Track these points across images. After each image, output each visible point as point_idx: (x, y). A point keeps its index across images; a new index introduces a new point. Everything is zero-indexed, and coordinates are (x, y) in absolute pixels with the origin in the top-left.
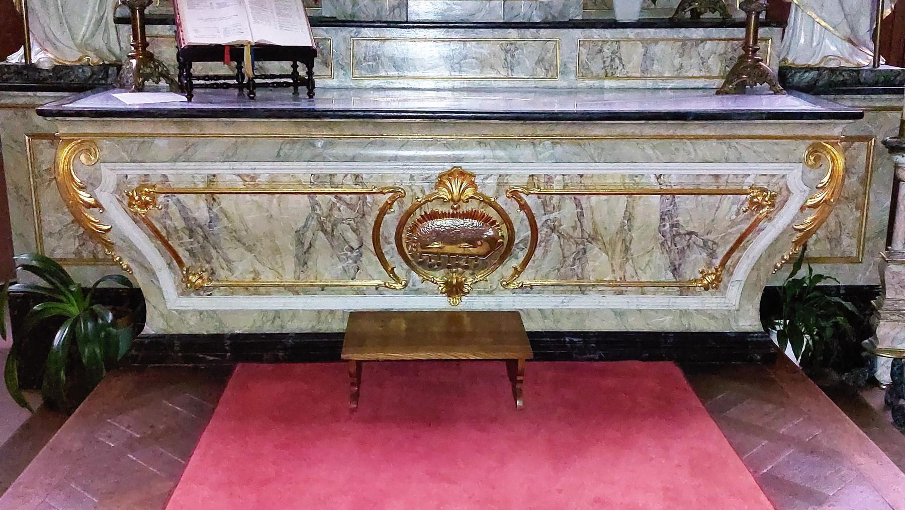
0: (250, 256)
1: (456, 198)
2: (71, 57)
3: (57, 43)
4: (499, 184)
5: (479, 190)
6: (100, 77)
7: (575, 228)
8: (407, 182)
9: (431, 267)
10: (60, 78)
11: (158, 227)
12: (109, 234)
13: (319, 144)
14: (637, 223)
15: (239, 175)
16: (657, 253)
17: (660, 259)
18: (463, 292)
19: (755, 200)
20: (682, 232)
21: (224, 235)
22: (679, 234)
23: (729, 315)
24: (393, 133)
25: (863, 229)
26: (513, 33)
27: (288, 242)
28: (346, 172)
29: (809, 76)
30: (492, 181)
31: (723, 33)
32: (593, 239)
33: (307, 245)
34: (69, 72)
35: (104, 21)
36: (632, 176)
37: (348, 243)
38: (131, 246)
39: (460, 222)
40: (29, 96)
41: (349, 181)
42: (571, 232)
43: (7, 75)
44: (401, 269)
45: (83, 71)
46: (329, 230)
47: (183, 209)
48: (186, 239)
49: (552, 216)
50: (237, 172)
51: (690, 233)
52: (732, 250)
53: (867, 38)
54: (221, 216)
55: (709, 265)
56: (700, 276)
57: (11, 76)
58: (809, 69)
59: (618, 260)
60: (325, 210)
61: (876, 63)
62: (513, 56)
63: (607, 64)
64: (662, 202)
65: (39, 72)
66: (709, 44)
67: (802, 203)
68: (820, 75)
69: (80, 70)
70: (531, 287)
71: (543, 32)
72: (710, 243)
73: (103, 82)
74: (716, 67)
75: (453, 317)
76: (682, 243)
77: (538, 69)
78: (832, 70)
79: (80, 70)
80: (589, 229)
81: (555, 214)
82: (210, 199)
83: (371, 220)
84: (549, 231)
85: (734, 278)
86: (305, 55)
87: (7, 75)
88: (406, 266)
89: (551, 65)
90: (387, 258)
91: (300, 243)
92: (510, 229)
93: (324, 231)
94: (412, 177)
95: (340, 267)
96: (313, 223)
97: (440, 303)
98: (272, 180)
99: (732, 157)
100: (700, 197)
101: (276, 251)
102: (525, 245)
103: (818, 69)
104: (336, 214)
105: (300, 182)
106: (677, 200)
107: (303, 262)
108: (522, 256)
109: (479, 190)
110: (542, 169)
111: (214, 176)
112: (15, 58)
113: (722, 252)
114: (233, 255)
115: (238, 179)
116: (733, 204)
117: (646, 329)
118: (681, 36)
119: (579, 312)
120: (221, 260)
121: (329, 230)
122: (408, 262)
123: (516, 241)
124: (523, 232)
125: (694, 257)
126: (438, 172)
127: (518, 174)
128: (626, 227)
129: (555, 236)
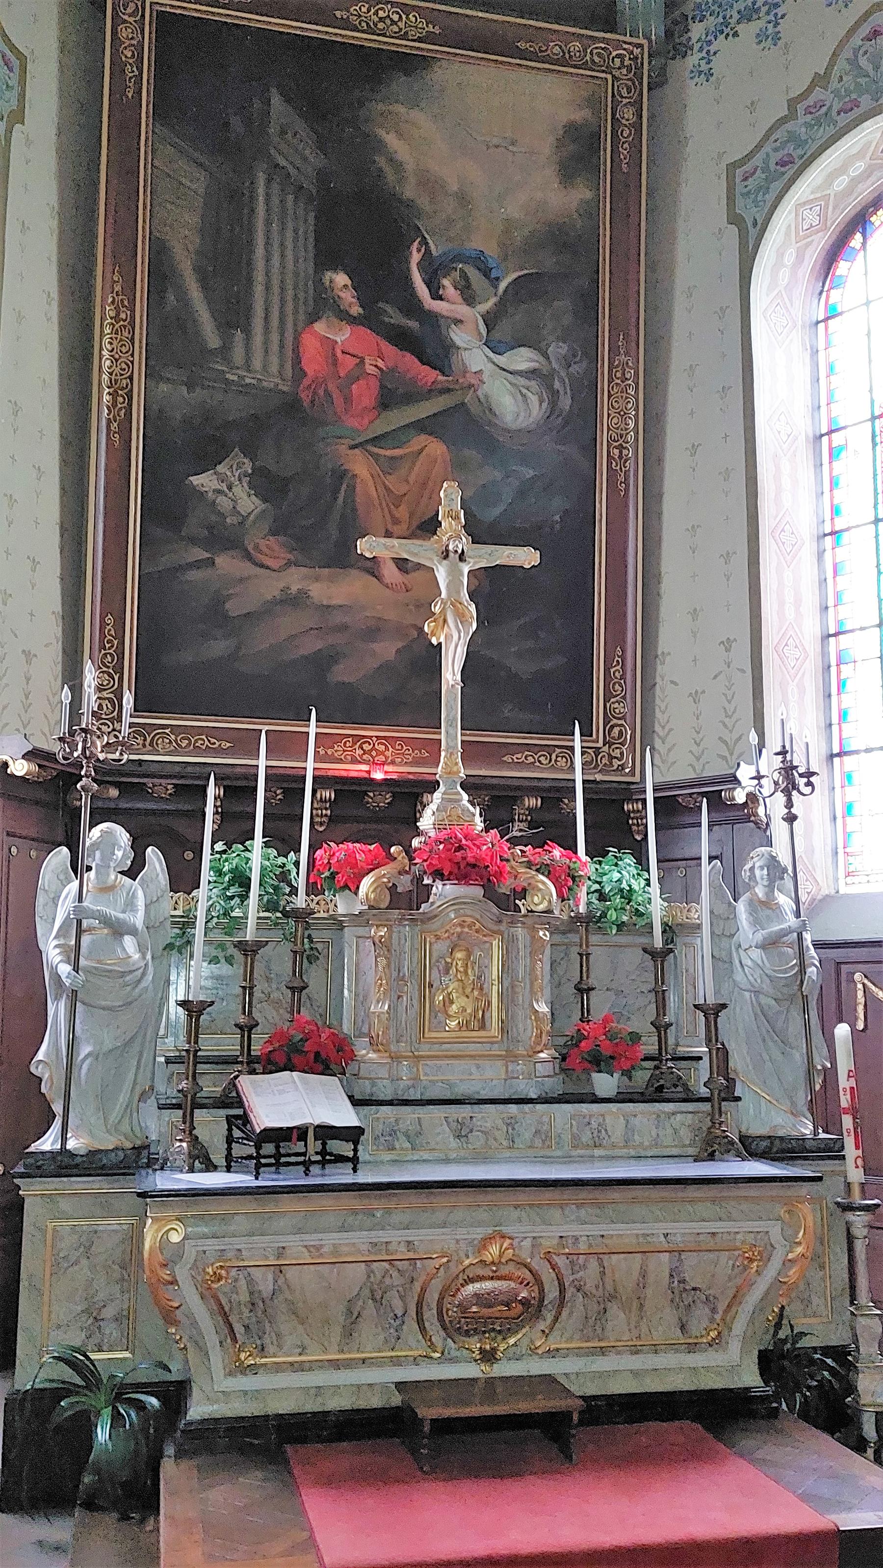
0: (300, 1328)
1: (496, 1261)
2: (108, 1142)
4: (533, 1246)
5: (517, 1252)
7: (597, 1287)
8: (453, 1246)
9: (467, 1334)
11: (224, 1301)
12: (177, 1312)
13: (378, 1214)
14: (651, 1278)
15: (306, 1246)
16: (668, 1310)
17: (670, 1316)
18: (495, 1359)
19: (747, 1255)
20: (687, 1288)
21: (283, 1307)
22: (685, 1290)
23: (733, 1369)
26: (513, 1108)
27: (338, 1312)
28: (400, 1239)
29: (764, 1144)
30: (527, 1243)
31: (690, 1107)
32: (613, 1297)
33: (355, 1314)
36: (645, 1235)
37: (393, 1311)
38: (194, 1324)
39: (497, 1284)
41: (403, 1248)
42: (594, 1291)
43: (41, 1162)
44: (438, 1336)
46: (378, 1297)
47: (250, 1282)
48: (246, 1313)
49: (578, 1276)
50: (305, 1243)
51: (694, 1289)
52: (729, 1306)
53: (805, 1109)
54: (285, 1287)
55: (712, 1320)
56: (704, 1332)
58: (762, 1138)
59: (634, 1319)
60: (379, 1277)
61: (816, 1133)
62: (513, 1129)
63: (595, 1135)
64: (670, 1261)
66: (679, 1117)
67: (783, 1258)
68: (772, 1143)
69: (113, 1154)
70: (557, 1350)
71: (538, 1106)
72: (711, 1298)
74: (686, 1135)
75: (491, 1382)
76: (688, 1299)
77: (536, 1141)
78: (781, 1139)
79: (113, 1154)
80: (609, 1287)
81: (581, 1273)
82: (277, 1271)
83: (417, 1286)
84: (575, 1290)
85: (735, 1332)
86: (353, 1135)
88: (442, 1333)
89: (546, 1137)
90: (427, 1324)
91: (350, 1312)
92: (542, 1291)
93: (374, 1299)
94: (457, 1241)
95: (382, 1337)
96: (366, 1292)
97: (472, 1371)
98: (335, 1251)
99: (724, 1216)
100: (701, 1254)
101: (327, 1322)
102: (553, 1307)
103: (769, 1137)
104: (388, 1281)
105: (359, 1252)
106: (683, 1257)
107: (348, 1333)
108: (550, 1317)
109: (517, 1252)
110: (571, 1230)
111: (284, 1248)
112: (48, 1143)
113: (721, 1307)
114: (284, 1328)
115: (304, 1250)
116: (729, 1258)
117: (660, 1389)
118: (655, 1109)
119: (601, 1375)
120: (273, 1334)
121: (378, 1297)
122: (445, 1329)
123: (546, 1302)
124: (552, 1293)
125: (698, 1312)
126: (481, 1236)
127: (549, 1236)
128: (641, 1285)
129: (579, 1295)
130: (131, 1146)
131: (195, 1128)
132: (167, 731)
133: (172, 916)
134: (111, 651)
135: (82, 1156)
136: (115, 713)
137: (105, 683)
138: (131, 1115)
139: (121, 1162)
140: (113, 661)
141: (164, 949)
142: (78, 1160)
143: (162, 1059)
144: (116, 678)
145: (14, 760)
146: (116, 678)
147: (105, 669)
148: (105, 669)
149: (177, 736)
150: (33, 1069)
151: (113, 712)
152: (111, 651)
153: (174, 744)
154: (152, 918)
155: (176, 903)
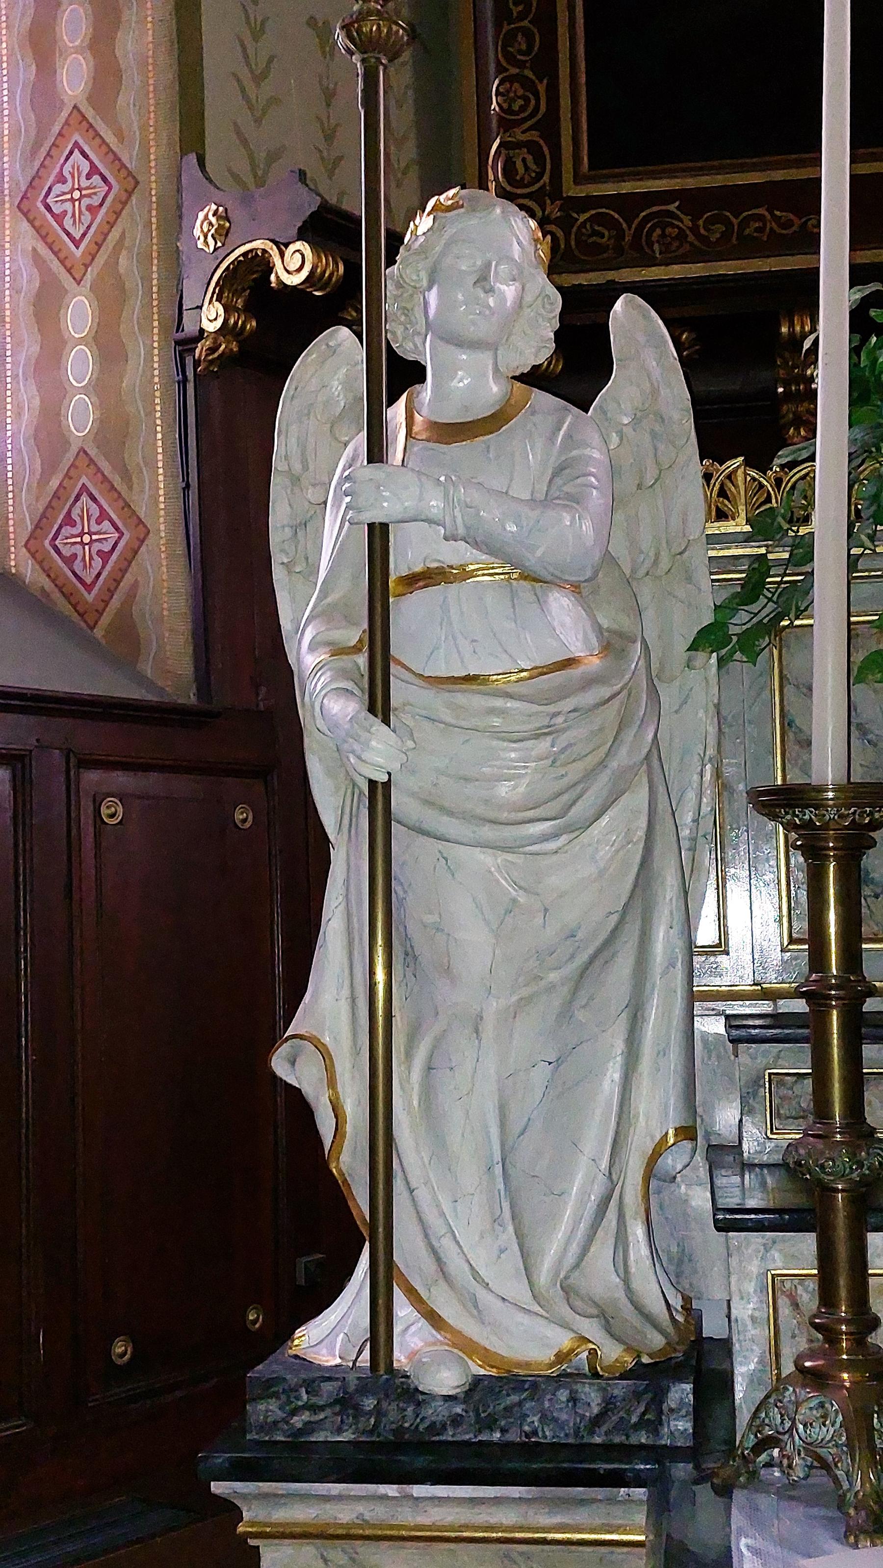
3: (482, 1295)
6: (634, 1419)
10: (490, 1424)
24: (592, 812)
25: (24, 1181)
34: (520, 1404)
35: (613, 1203)
40: (384, 1497)
43: (306, 1416)
45: (573, 1399)
57: (322, 1416)
65: (419, 1404)
69: (563, 1395)
73: (643, 1438)
87: (306, 1416)
117: (273, 521)
130: (629, 1361)
131: (875, 1323)
132: (672, 207)
133: (713, 540)
134: (525, 23)
135: (448, 1398)
136: (546, 178)
137: (516, 107)
138: (621, 1239)
139: (596, 1422)
140: (530, 47)
141: (693, 647)
142: (436, 1412)
143: (717, 1026)
144: (542, 88)
145: (282, 246)
146: (542, 88)
147: (514, 71)
148: (514, 71)
149: (695, 219)
150: (279, 1065)
151: (540, 176)
152: (525, 23)
153: (691, 238)
154: (644, 546)
155: (722, 493)
